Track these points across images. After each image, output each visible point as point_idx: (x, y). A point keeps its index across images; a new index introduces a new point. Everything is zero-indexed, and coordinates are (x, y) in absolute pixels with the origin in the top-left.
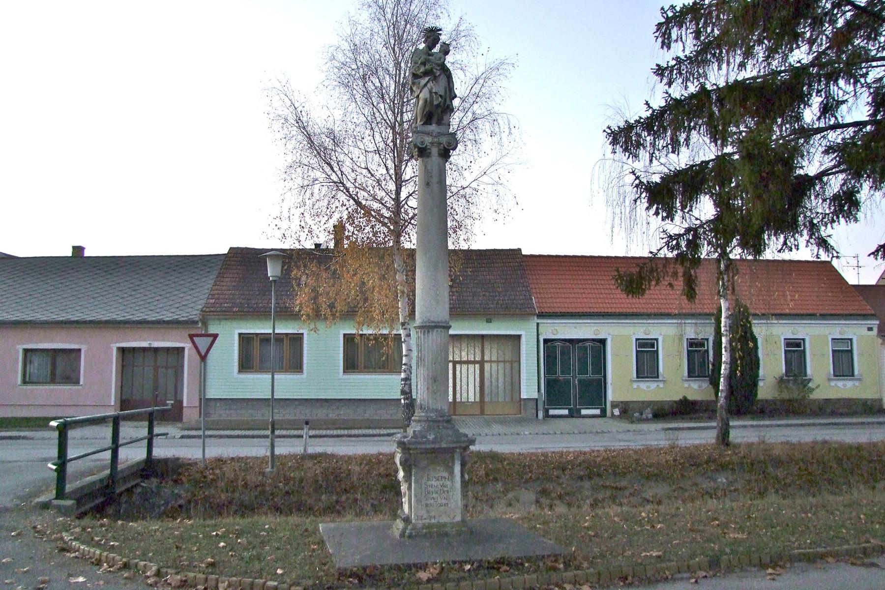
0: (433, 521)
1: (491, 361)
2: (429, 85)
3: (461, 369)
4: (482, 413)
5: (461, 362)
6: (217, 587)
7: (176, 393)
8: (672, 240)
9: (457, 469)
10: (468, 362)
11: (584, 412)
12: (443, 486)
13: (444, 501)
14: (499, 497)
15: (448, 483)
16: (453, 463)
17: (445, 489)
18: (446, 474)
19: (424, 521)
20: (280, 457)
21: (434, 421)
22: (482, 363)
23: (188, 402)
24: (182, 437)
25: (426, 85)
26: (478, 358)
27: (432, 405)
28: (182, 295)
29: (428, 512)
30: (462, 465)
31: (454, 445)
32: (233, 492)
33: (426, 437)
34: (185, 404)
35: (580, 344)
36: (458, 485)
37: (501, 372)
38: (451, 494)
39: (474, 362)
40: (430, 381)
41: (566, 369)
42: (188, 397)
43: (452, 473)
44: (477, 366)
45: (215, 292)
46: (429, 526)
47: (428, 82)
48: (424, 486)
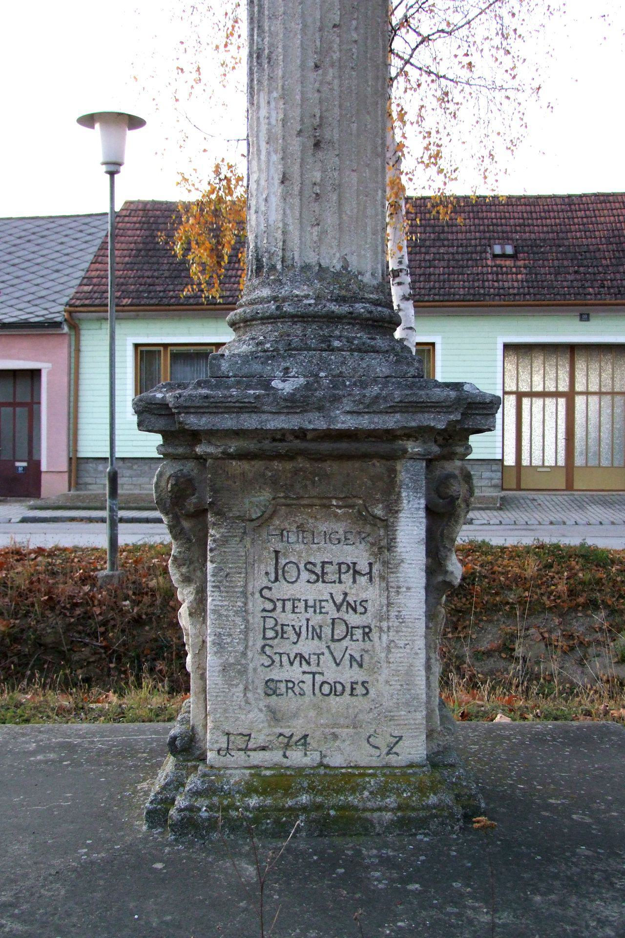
0: (297, 758)
1: (587, 393)
3: (533, 408)
4: (570, 486)
5: (532, 395)
7: (30, 453)
8: (604, 608)
9: (410, 530)
10: (544, 395)
12: (345, 604)
13: (349, 675)
14: (598, 643)
15: (368, 592)
16: (393, 510)
17: (354, 619)
18: (358, 554)
19: (257, 758)
20: (127, 549)
21: (303, 318)
22: (570, 396)
23: (48, 463)
24: (24, 520)
26: (564, 387)
27: (304, 253)
28: (39, 281)
29: (275, 716)
30: (430, 511)
31: (391, 422)
32: (26, 615)
33: (266, 384)
34: (44, 467)
36: (413, 601)
37: (606, 412)
38: (379, 641)
39: (556, 394)
40: (295, 145)
42: (51, 456)
43: (384, 549)
44: (562, 401)
45: (94, 274)
46: (278, 782)
48: (257, 604)
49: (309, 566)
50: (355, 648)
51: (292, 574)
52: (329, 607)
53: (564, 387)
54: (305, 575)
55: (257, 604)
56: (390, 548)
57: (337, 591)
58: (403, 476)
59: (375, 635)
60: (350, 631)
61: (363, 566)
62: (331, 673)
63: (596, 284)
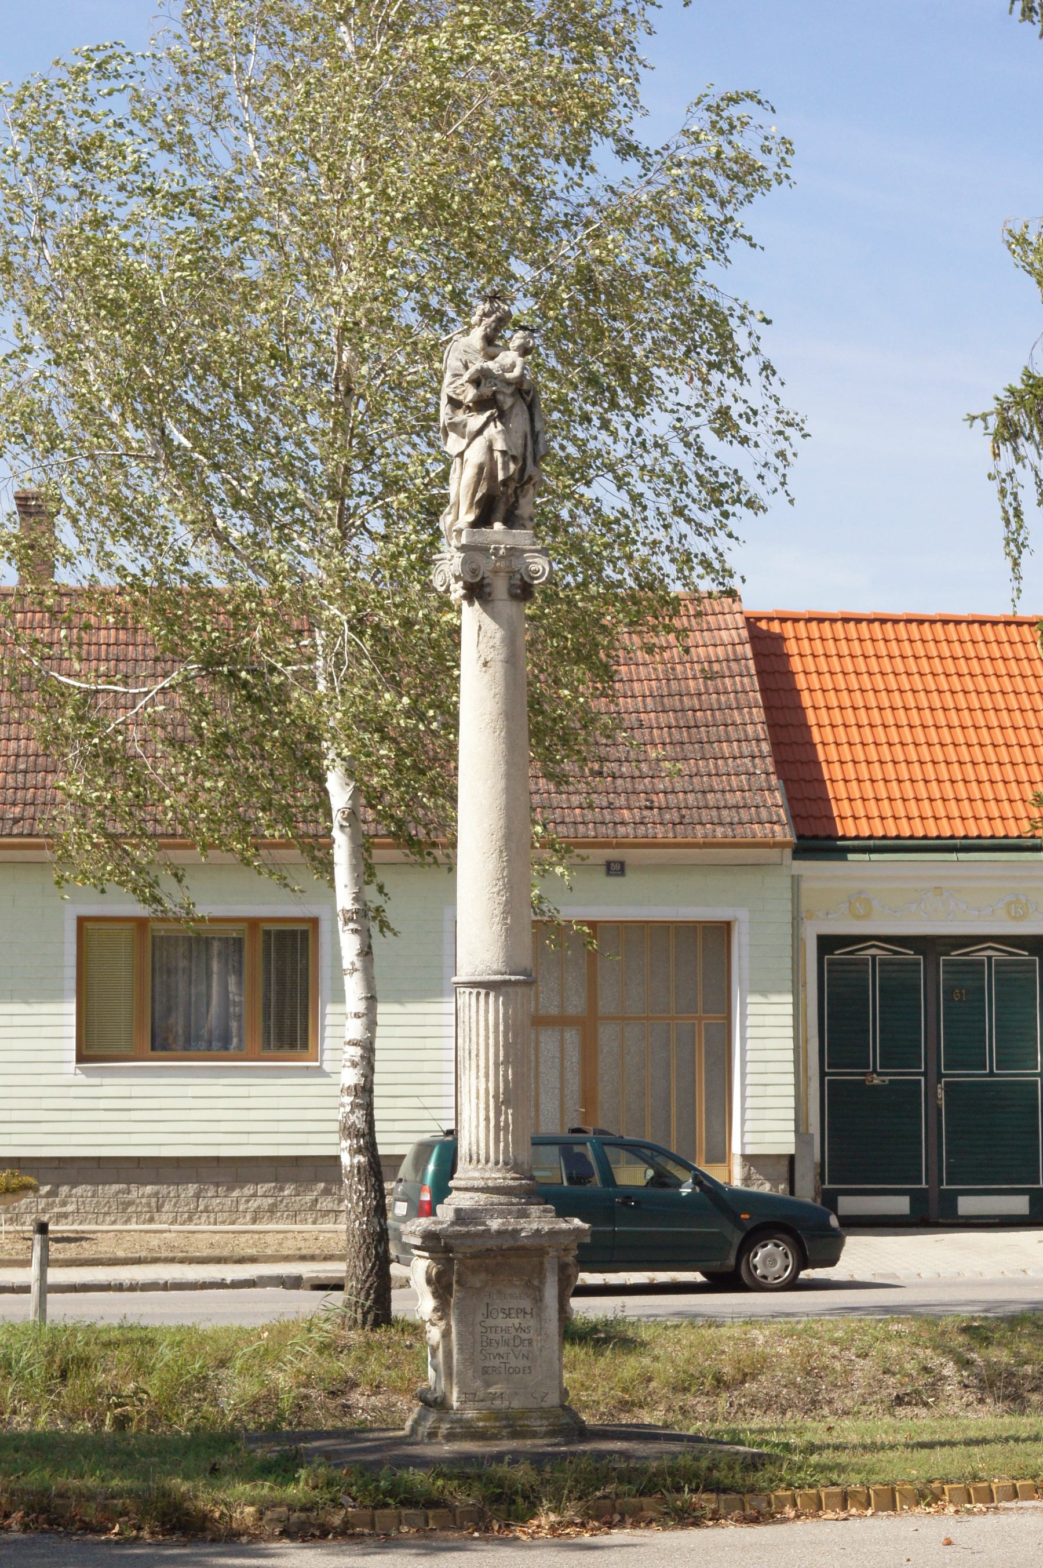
2: (486, 433)
6: (1041, 800)
11: (967, 1205)
13: (522, 1363)
15: (531, 1322)
16: (542, 1282)
17: (524, 1336)
18: (526, 1304)
22: (587, 1025)
25: (480, 432)
26: (576, 1005)
35: (955, 955)
39: (561, 1022)
41: (900, 1052)
43: (539, 1301)
44: (572, 1036)
47: (486, 425)
49: (503, 1310)
50: (524, 1349)
51: (494, 1315)
52: (512, 1330)
53: (576, 1005)
54: (501, 1315)
55: (479, 1329)
56: (541, 1300)
57: (516, 1321)
58: (547, 1266)
59: (534, 1343)
60: (522, 1341)
61: (528, 1310)
62: (513, 1363)
63: (634, 801)
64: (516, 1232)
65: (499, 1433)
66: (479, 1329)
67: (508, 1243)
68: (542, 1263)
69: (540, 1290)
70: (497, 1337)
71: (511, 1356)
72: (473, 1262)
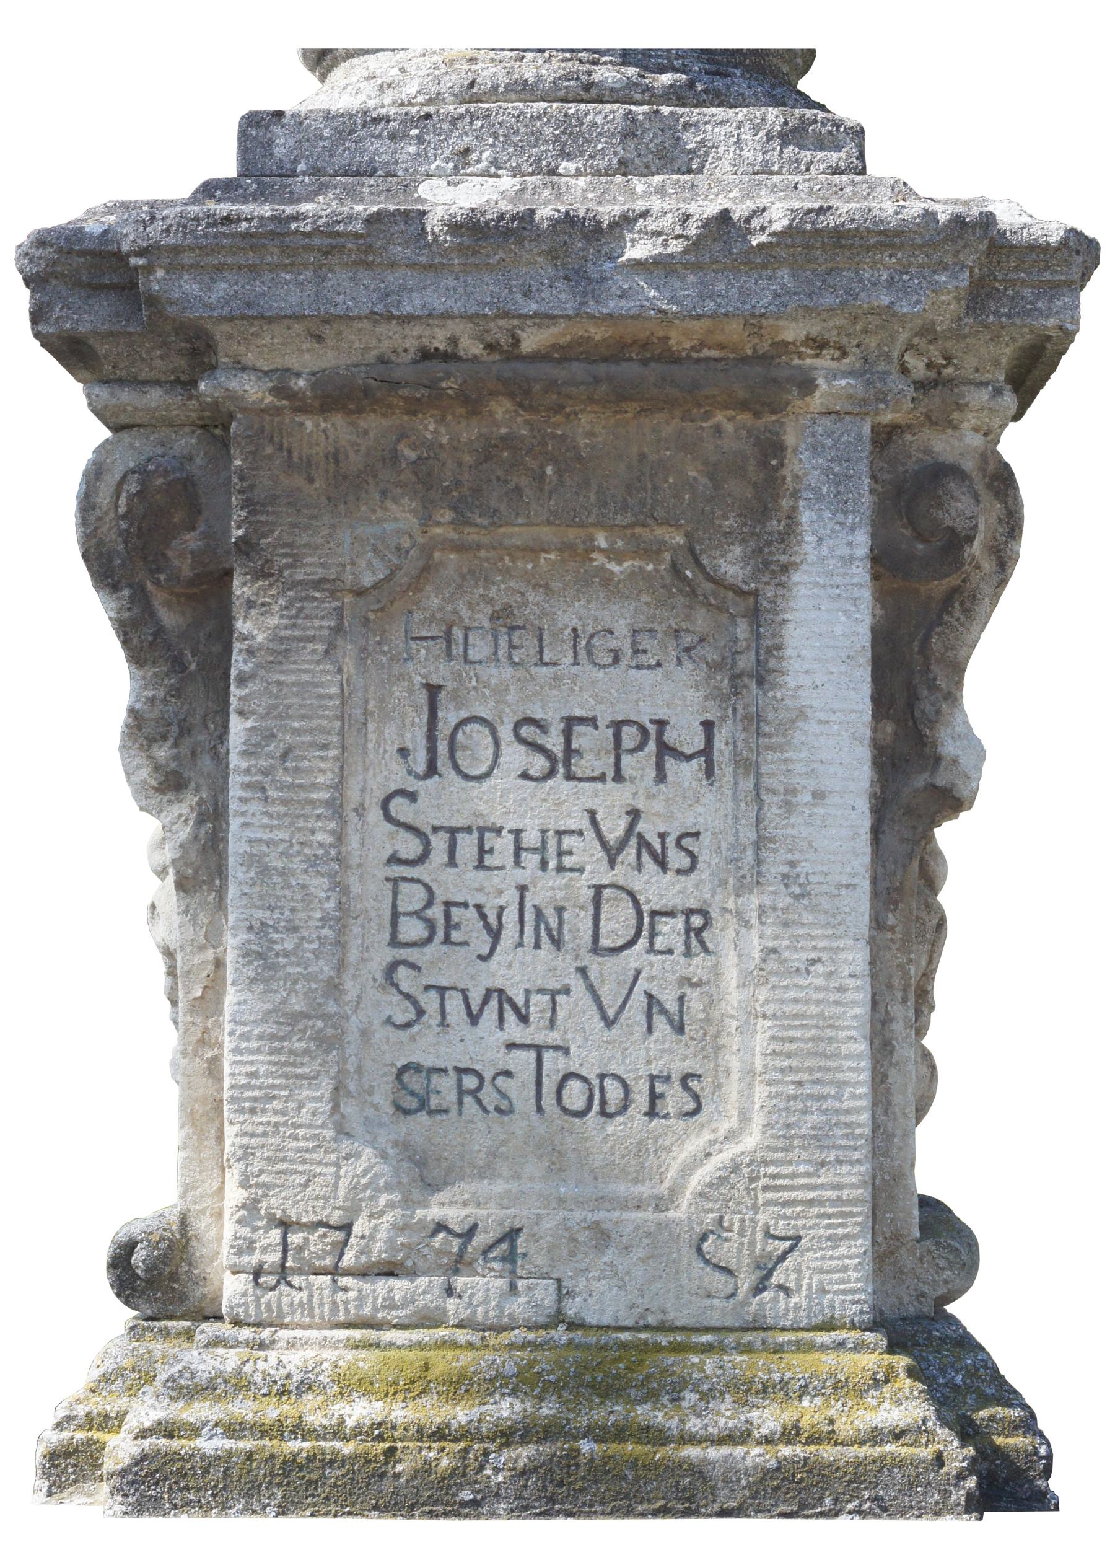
13: (642, 1053)
15: (689, 802)
16: (773, 558)
17: (658, 888)
18: (675, 696)
52: (586, 852)
54: (515, 756)
55: (373, 840)
57: (611, 804)
58: (804, 464)
60: (646, 921)
64: (584, 240)
65: (459, 1475)
66: (373, 840)
67: (545, 311)
68: (772, 449)
69: (755, 609)
70: (498, 889)
71: (576, 1005)
72: (336, 428)
